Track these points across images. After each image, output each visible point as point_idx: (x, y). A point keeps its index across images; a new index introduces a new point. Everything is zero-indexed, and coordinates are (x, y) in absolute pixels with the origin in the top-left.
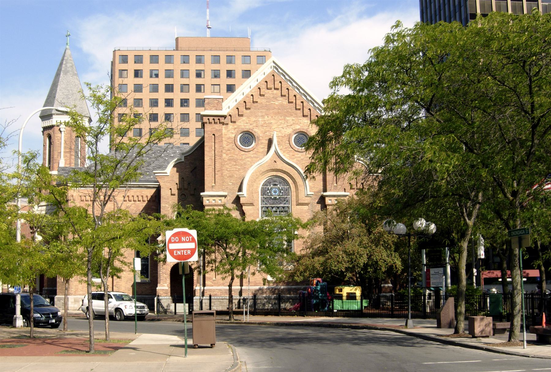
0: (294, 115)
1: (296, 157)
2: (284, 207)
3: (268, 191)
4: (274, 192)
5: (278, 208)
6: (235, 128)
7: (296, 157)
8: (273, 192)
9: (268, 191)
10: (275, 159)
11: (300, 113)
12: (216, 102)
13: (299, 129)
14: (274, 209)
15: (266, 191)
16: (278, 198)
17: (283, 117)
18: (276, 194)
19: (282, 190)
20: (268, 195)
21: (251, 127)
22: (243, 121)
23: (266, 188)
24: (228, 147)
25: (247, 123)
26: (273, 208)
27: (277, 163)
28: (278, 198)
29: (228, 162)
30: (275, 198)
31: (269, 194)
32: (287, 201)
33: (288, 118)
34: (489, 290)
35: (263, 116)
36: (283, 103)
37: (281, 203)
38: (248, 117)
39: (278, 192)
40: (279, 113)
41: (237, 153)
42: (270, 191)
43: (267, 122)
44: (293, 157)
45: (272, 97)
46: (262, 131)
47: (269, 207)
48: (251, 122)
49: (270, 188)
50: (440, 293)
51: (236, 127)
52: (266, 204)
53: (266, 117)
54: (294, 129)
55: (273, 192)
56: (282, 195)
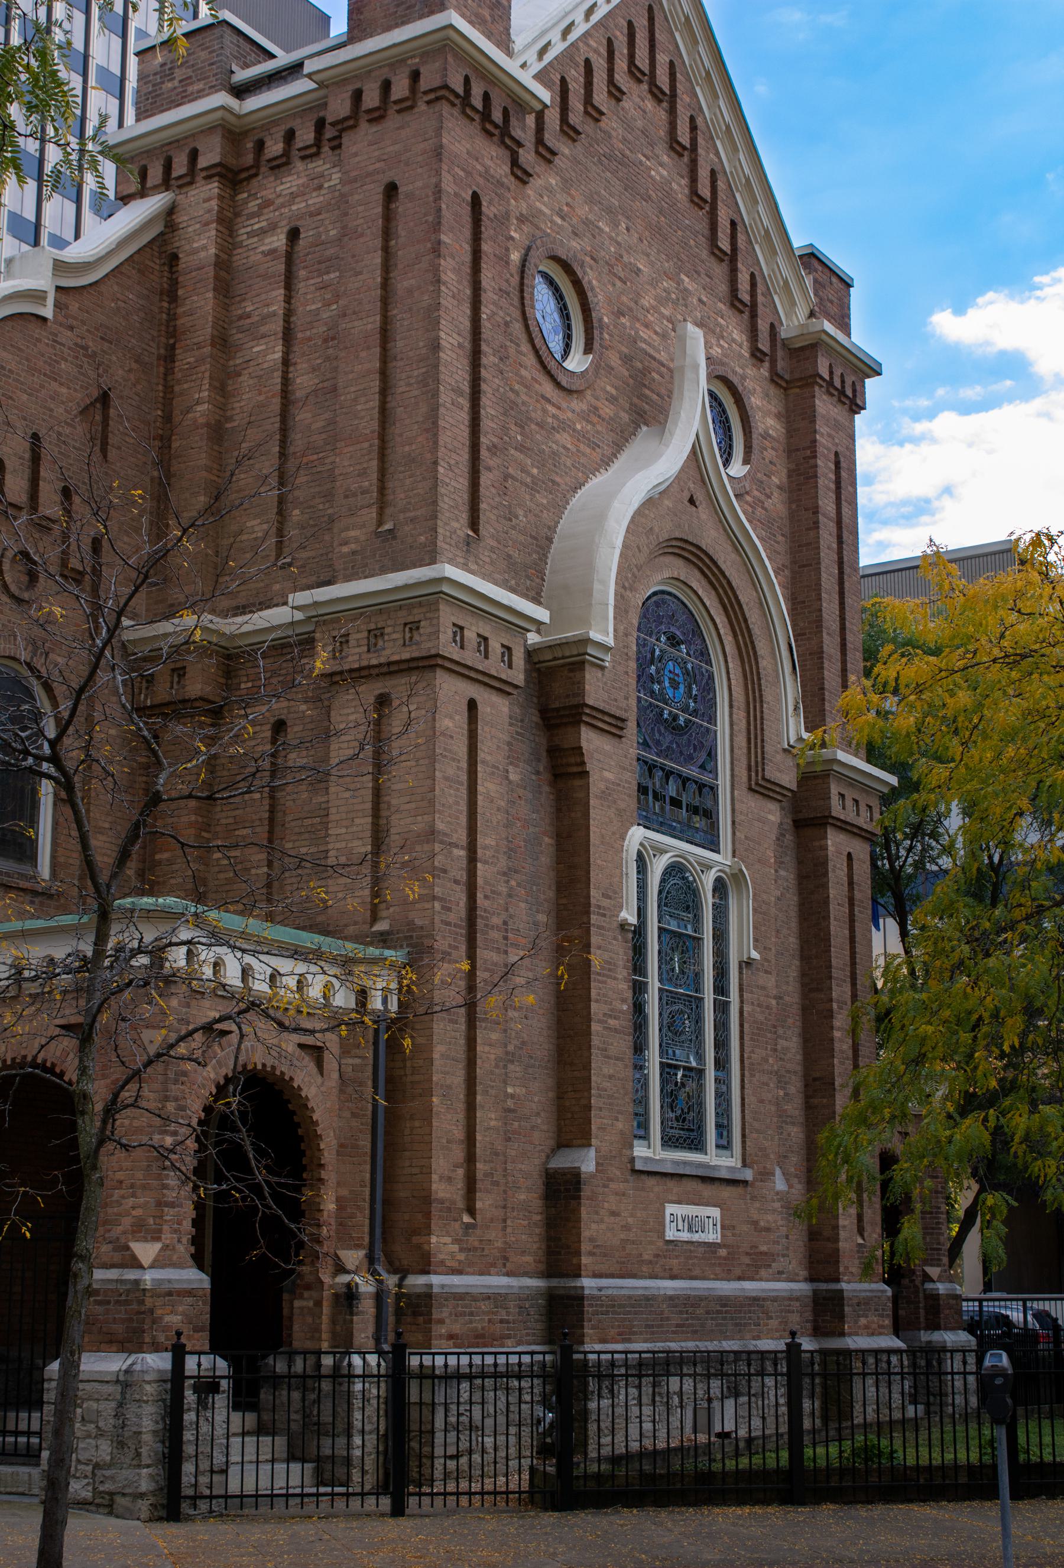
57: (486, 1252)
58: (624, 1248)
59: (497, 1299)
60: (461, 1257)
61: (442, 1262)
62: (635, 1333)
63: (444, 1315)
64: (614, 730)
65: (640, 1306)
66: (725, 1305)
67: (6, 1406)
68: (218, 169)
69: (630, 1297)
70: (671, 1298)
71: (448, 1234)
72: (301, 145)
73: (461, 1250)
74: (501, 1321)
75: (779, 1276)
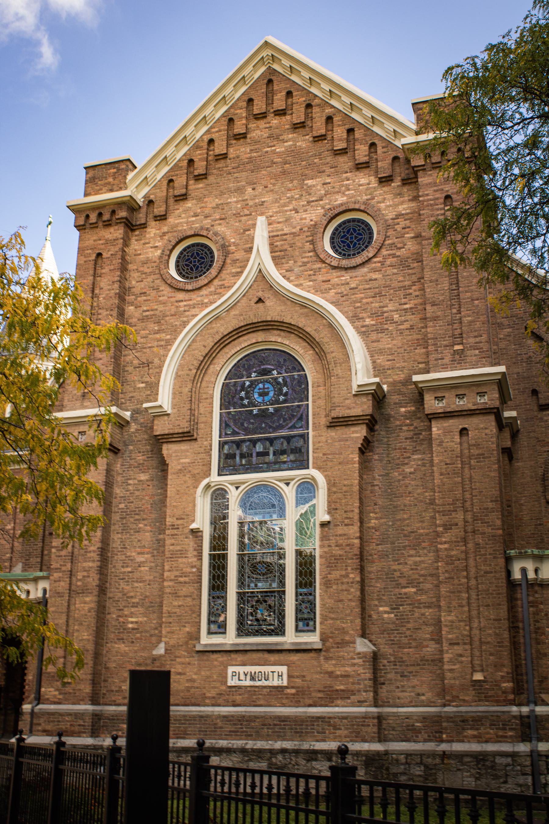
0: (328, 170)
1: (334, 286)
2: (288, 439)
3: (243, 394)
4: (260, 395)
5: (271, 441)
6: (164, 234)
7: (334, 286)
8: (256, 395)
9: (243, 394)
10: (260, 294)
11: (344, 162)
12: (113, 171)
13: (342, 205)
14: (259, 448)
15: (237, 392)
16: (271, 410)
17: (295, 182)
18: (267, 398)
19: (285, 384)
20: (243, 406)
21: (207, 222)
22: (186, 211)
23: (235, 384)
24: (142, 285)
25: (196, 215)
26: (254, 442)
27: (268, 303)
28: (271, 410)
29: (140, 325)
30: (263, 414)
31: (246, 402)
32: (301, 419)
33: (310, 182)
34: (323, 796)
35: (240, 190)
36: (298, 144)
37: (281, 427)
38: (200, 200)
39: (271, 394)
40: (284, 173)
41: (165, 298)
42: (247, 393)
43: (251, 203)
44: (327, 286)
45: (266, 135)
46: (236, 231)
47: (243, 441)
48: (207, 211)
49: (247, 383)
50: (168, 742)
51: (165, 229)
52: (235, 433)
53: (250, 190)
54: (328, 207)
55: (256, 395)
56: (285, 401)
57: (77, 694)
58: (189, 691)
59: (77, 715)
60: (61, 697)
61: (48, 699)
62: (188, 734)
63: (41, 722)
64: (189, 438)
65: (195, 720)
66: (284, 721)
67: (3, 736)
68: (124, 220)
69: (184, 716)
70: (225, 717)
71: (52, 687)
72: (117, 217)
73: (60, 694)
74: (79, 725)
75: (360, 703)
